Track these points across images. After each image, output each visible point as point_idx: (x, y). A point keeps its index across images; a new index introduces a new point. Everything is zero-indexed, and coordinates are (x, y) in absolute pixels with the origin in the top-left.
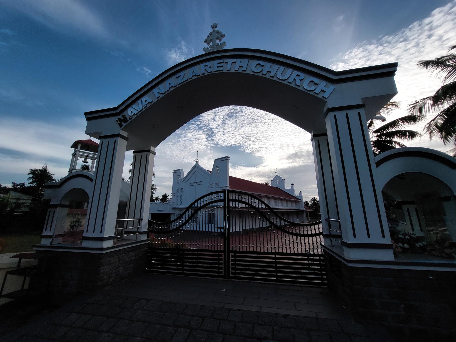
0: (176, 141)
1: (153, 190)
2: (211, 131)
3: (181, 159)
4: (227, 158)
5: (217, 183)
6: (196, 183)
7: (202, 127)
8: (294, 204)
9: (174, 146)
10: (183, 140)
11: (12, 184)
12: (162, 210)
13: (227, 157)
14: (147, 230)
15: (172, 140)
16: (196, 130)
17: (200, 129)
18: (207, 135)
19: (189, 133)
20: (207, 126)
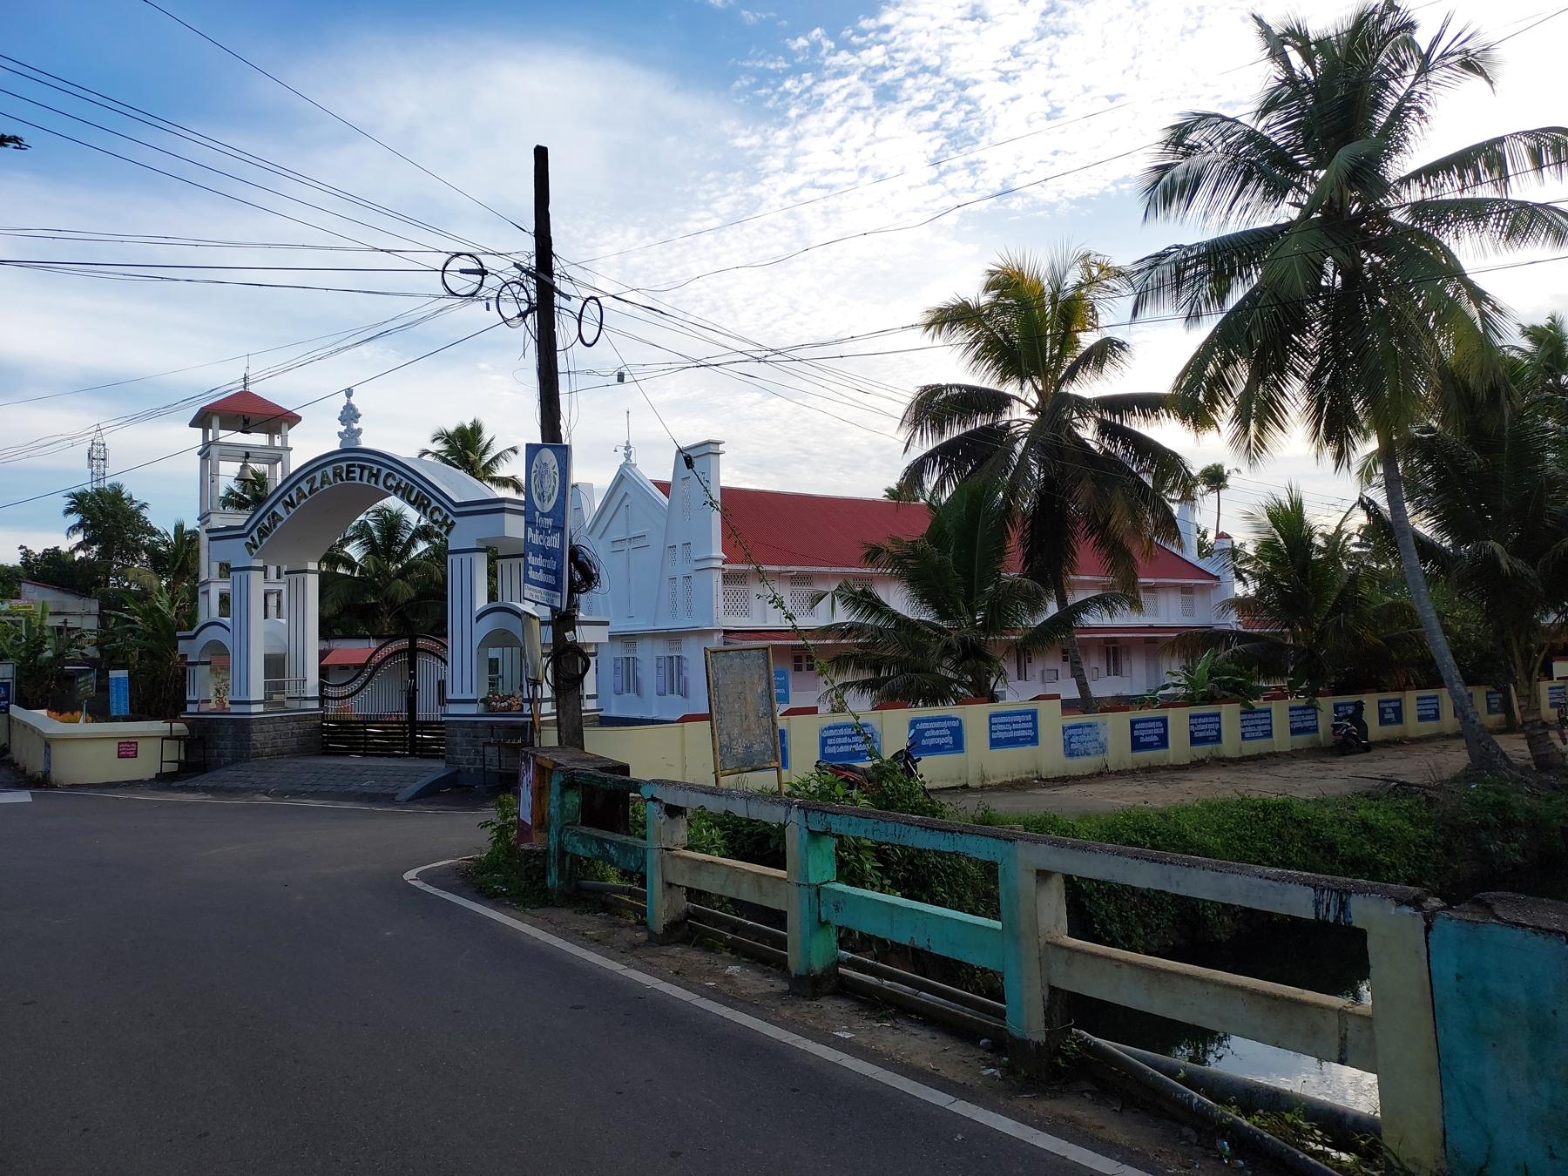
0: (737, 204)
2: (961, 100)
3: (775, 321)
7: (897, 85)
9: (728, 235)
10: (783, 188)
11: (22, 556)
13: (708, 443)
14: (318, 695)
15: (714, 200)
16: (858, 109)
17: (887, 95)
18: (937, 133)
19: (817, 135)
20: (936, 72)
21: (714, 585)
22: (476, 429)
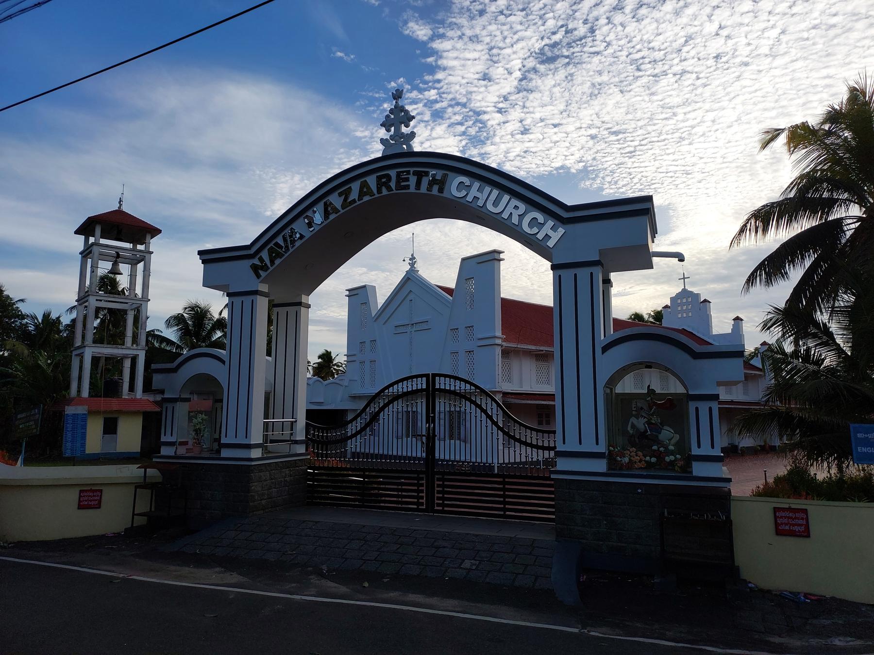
6: (413, 324)
12: (322, 401)
21: (497, 357)
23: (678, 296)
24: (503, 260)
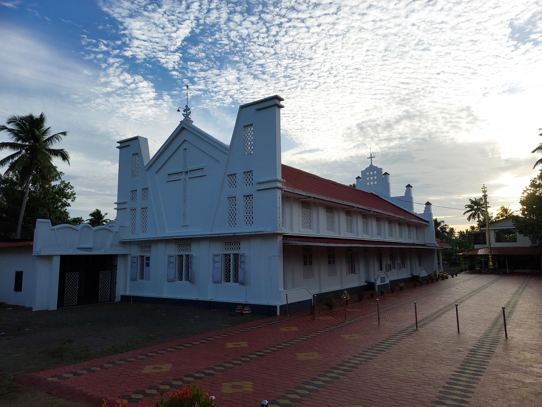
1: (67, 199)
4: (277, 101)
5: (249, 172)
6: (187, 172)
8: (414, 231)
12: (90, 246)
21: (278, 200)
22: (41, 119)
23: (368, 170)
24: (283, 107)
